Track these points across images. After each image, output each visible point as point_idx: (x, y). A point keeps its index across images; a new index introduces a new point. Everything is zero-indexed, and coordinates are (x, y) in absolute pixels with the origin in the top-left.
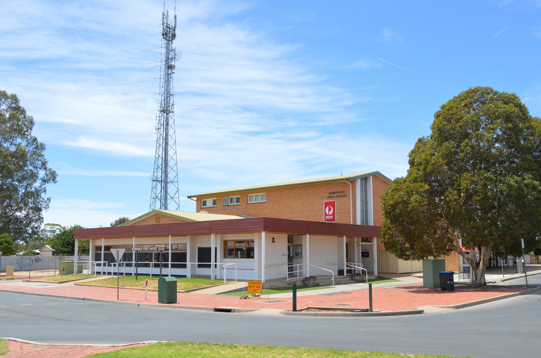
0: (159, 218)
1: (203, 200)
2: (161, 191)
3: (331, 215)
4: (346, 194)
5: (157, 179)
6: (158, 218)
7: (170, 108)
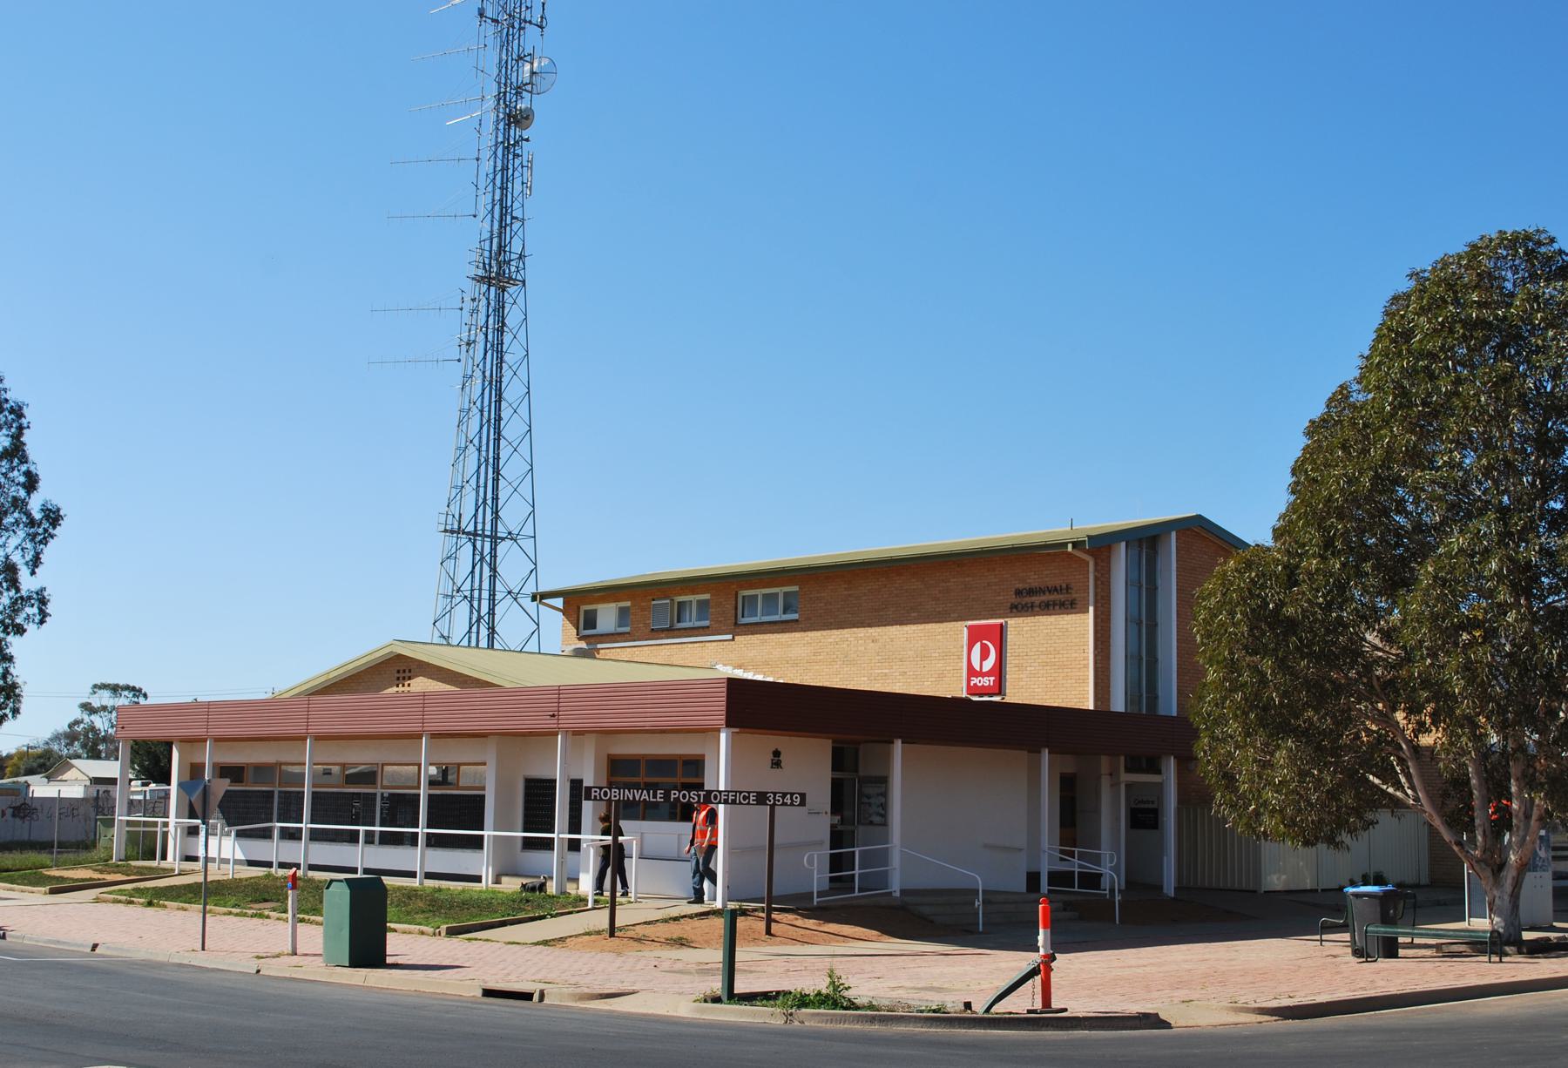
0: (407, 671)
1: (584, 608)
2: (472, 572)
3: (988, 674)
4: (1074, 596)
5: (459, 527)
6: (404, 671)
7: (513, 269)
